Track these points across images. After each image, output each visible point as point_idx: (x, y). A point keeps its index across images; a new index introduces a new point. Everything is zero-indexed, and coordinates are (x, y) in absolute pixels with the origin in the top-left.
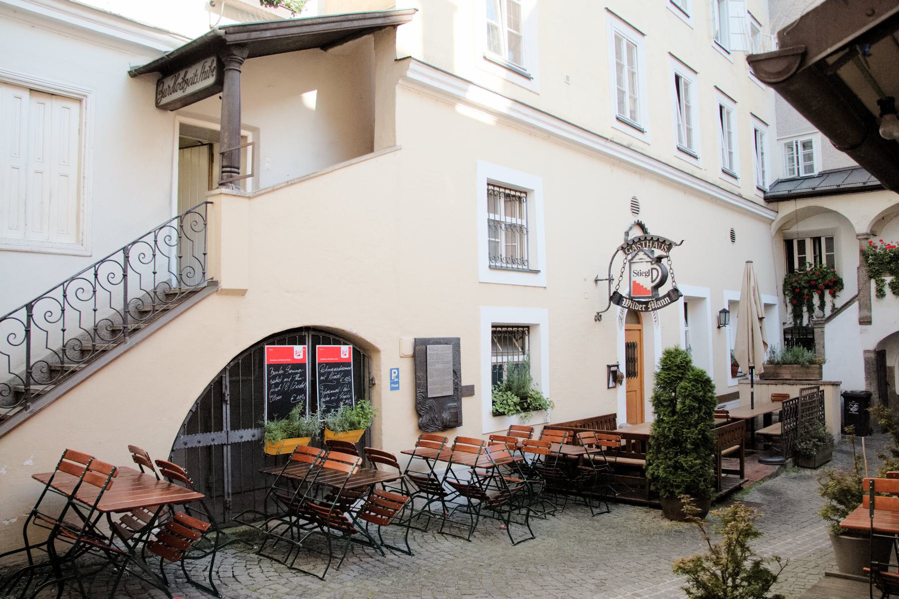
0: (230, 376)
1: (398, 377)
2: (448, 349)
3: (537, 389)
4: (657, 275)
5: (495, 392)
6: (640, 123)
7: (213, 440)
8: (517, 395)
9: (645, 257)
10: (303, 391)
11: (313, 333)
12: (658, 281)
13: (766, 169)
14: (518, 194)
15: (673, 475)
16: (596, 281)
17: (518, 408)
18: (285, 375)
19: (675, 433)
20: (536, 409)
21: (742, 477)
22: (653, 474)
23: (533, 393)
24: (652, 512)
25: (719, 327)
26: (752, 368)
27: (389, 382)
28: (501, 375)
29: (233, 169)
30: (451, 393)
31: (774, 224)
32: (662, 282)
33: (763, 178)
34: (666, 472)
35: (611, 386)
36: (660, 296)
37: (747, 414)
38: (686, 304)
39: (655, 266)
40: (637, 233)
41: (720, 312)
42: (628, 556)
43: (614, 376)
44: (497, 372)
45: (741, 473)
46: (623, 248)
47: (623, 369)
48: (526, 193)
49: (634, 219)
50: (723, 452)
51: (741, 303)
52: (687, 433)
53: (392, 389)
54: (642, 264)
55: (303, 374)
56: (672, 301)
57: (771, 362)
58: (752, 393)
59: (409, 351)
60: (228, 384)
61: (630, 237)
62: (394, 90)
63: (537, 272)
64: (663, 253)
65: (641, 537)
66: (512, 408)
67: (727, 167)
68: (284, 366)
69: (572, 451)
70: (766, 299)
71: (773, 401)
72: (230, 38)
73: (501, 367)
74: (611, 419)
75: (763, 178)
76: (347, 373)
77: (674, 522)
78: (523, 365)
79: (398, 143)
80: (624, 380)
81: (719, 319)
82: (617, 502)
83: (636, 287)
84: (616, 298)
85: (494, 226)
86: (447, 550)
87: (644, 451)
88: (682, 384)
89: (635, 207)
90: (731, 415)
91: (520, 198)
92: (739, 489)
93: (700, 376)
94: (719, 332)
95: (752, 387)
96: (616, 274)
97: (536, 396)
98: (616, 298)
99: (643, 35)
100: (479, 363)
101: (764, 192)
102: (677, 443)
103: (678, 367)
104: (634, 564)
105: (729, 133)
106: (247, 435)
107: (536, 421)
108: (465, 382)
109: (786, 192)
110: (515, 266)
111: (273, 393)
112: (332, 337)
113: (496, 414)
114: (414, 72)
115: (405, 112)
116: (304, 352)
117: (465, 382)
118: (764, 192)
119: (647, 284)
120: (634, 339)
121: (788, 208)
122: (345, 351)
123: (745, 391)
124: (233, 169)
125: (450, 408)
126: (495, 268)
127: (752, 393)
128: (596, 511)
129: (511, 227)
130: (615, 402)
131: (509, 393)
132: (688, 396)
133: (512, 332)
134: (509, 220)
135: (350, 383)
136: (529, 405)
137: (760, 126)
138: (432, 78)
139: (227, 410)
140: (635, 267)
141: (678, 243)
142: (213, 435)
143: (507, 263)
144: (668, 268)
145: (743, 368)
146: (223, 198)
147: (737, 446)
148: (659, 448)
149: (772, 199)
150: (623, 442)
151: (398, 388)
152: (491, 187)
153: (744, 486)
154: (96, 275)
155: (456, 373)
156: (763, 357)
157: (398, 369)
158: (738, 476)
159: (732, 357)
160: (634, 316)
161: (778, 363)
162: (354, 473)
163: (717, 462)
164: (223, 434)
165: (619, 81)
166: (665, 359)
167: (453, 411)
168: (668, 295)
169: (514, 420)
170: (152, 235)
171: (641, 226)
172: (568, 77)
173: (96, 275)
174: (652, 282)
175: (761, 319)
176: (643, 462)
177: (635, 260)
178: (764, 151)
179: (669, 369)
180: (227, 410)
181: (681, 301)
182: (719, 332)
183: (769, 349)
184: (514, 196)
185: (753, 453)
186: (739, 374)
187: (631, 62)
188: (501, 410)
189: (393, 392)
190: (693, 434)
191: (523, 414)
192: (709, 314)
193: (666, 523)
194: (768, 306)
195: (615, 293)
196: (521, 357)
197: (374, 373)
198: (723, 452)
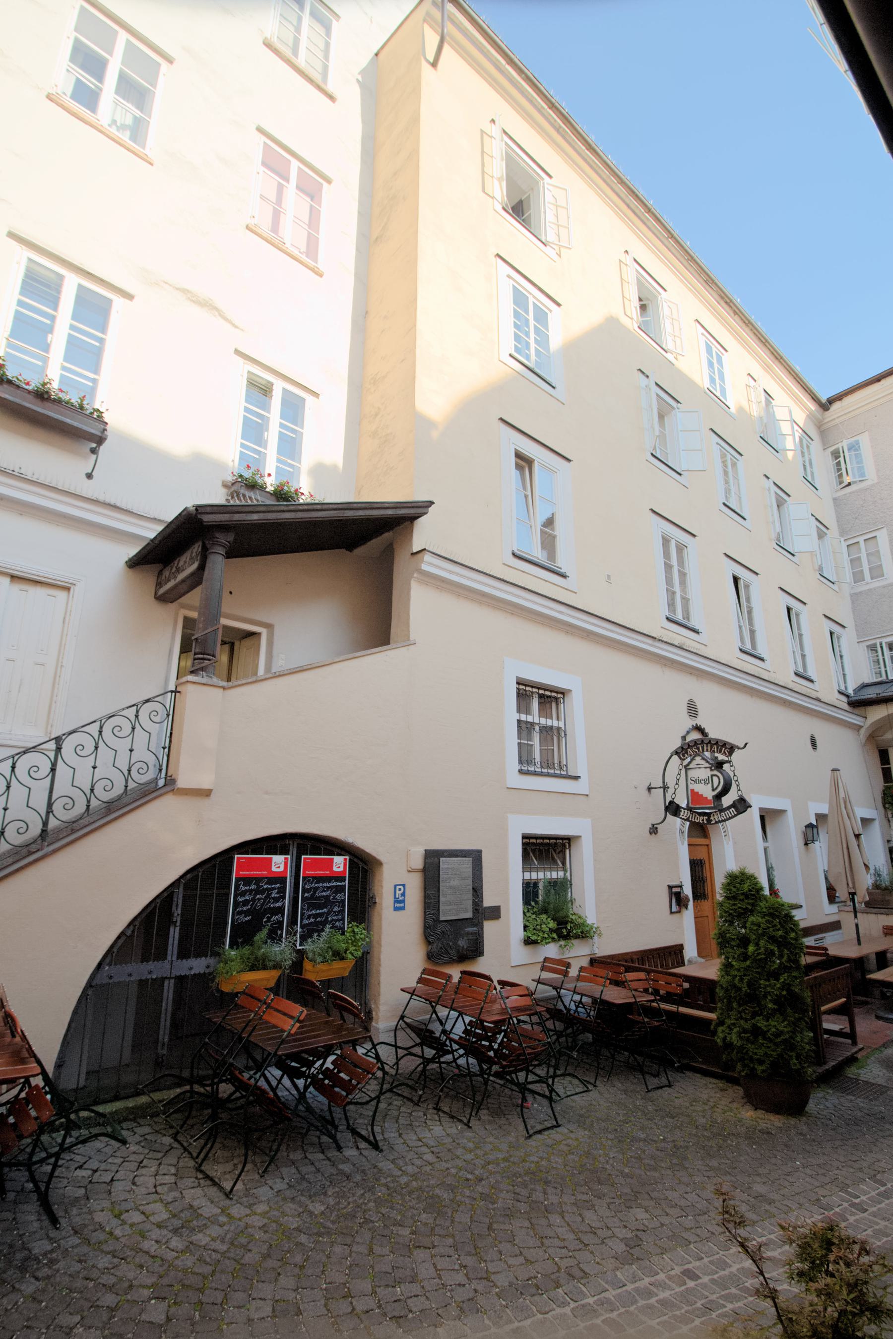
0: (185, 889)
1: (403, 894)
2: (466, 864)
3: (580, 913)
4: (718, 782)
5: (528, 915)
6: (693, 623)
7: (150, 972)
8: (554, 919)
9: (703, 762)
10: (281, 910)
11: (298, 841)
12: (719, 789)
13: (847, 671)
14: (553, 694)
15: (752, 1043)
16: (649, 789)
17: (555, 935)
18: (257, 892)
19: (750, 985)
20: (577, 937)
21: (855, 1043)
22: (725, 1039)
23: (574, 917)
24: (730, 1091)
25: (806, 844)
26: (853, 895)
27: (392, 900)
28: (536, 894)
29: (206, 656)
30: (469, 915)
31: (863, 731)
32: (726, 790)
33: (845, 683)
34: (742, 1039)
35: (674, 910)
36: (724, 807)
37: (852, 952)
38: (762, 818)
39: (715, 772)
40: (695, 736)
41: (807, 827)
42: (685, 1179)
43: (677, 898)
44: (530, 891)
45: (852, 1036)
46: (677, 753)
47: (688, 890)
48: (563, 694)
49: (690, 723)
50: (823, 1008)
51: (829, 817)
52: (766, 986)
53: (396, 909)
54: (701, 771)
55: (282, 891)
56: (739, 813)
57: (876, 886)
58: (857, 925)
59: (419, 863)
60: (180, 902)
61: (689, 739)
62: (410, 585)
63: (576, 778)
64: (726, 758)
65: (709, 1139)
66: (546, 936)
67: (801, 670)
68: (258, 880)
69: (616, 995)
70: (862, 812)
71: (886, 934)
72: (206, 518)
73: (536, 884)
74: (675, 953)
75: (845, 683)
76: (341, 889)
77: (760, 1113)
78: (561, 883)
79: (412, 637)
80: (691, 904)
81: (805, 835)
82: (684, 1068)
83: (695, 796)
84: (673, 809)
85: (524, 728)
86: (432, 1143)
87: (714, 1002)
88: (752, 919)
89: (692, 710)
90: (832, 952)
91: (556, 699)
92: (852, 1060)
93: (776, 909)
94: (807, 849)
95: (856, 917)
96: (670, 781)
97: (580, 921)
98: (673, 809)
99: (694, 536)
100: (506, 881)
101: (848, 696)
102: (753, 998)
103: (747, 896)
104: (692, 1197)
105: (800, 635)
106: (198, 965)
107: (578, 954)
108: (488, 902)
109: (874, 696)
110: (551, 771)
111: (240, 913)
112: (322, 847)
113: (528, 942)
114: (428, 564)
115: (421, 606)
116: (286, 864)
117: (488, 902)
118: (848, 696)
119: (707, 792)
120: (701, 854)
121: (877, 714)
122: (339, 863)
123: (848, 920)
124: (206, 656)
125: (468, 934)
126: (528, 773)
127: (857, 925)
128: (653, 1082)
129: (547, 731)
130: (683, 930)
131: (544, 916)
132: (763, 935)
133: (548, 844)
134: (543, 721)
135: (343, 901)
136: (569, 932)
137: (836, 629)
138: (451, 572)
139: (175, 933)
140: (691, 773)
141: (742, 746)
142: (151, 965)
143: (542, 767)
144: (732, 774)
145: (842, 893)
146: (190, 687)
147: (845, 999)
148: (730, 1002)
149: (858, 704)
150: (686, 985)
151: (403, 908)
152: (521, 687)
153: (859, 1056)
154: (13, 767)
155: (477, 892)
156: (866, 881)
157: (404, 885)
158: (849, 1041)
159: (826, 878)
160: (700, 830)
161: (886, 889)
162: (293, 1032)
163: (815, 1025)
164: (166, 964)
165: (669, 581)
166: (729, 884)
167: (470, 937)
168: (733, 805)
169: (551, 950)
170: (98, 724)
171: (698, 729)
172: (609, 576)
173: (13, 767)
174: (713, 790)
175: (857, 836)
176: (712, 1016)
177: (691, 766)
178: (843, 654)
179: (734, 898)
180: (175, 933)
181: (753, 814)
182: (807, 849)
183: (872, 871)
184: (550, 697)
185: (867, 1003)
186: (837, 900)
187: (681, 562)
188: (534, 938)
189: (396, 912)
190: (775, 988)
191: (562, 943)
192: (791, 829)
193: (748, 1114)
194: (866, 822)
195: (671, 802)
196: (561, 874)
197: (376, 889)
198: (823, 1008)
